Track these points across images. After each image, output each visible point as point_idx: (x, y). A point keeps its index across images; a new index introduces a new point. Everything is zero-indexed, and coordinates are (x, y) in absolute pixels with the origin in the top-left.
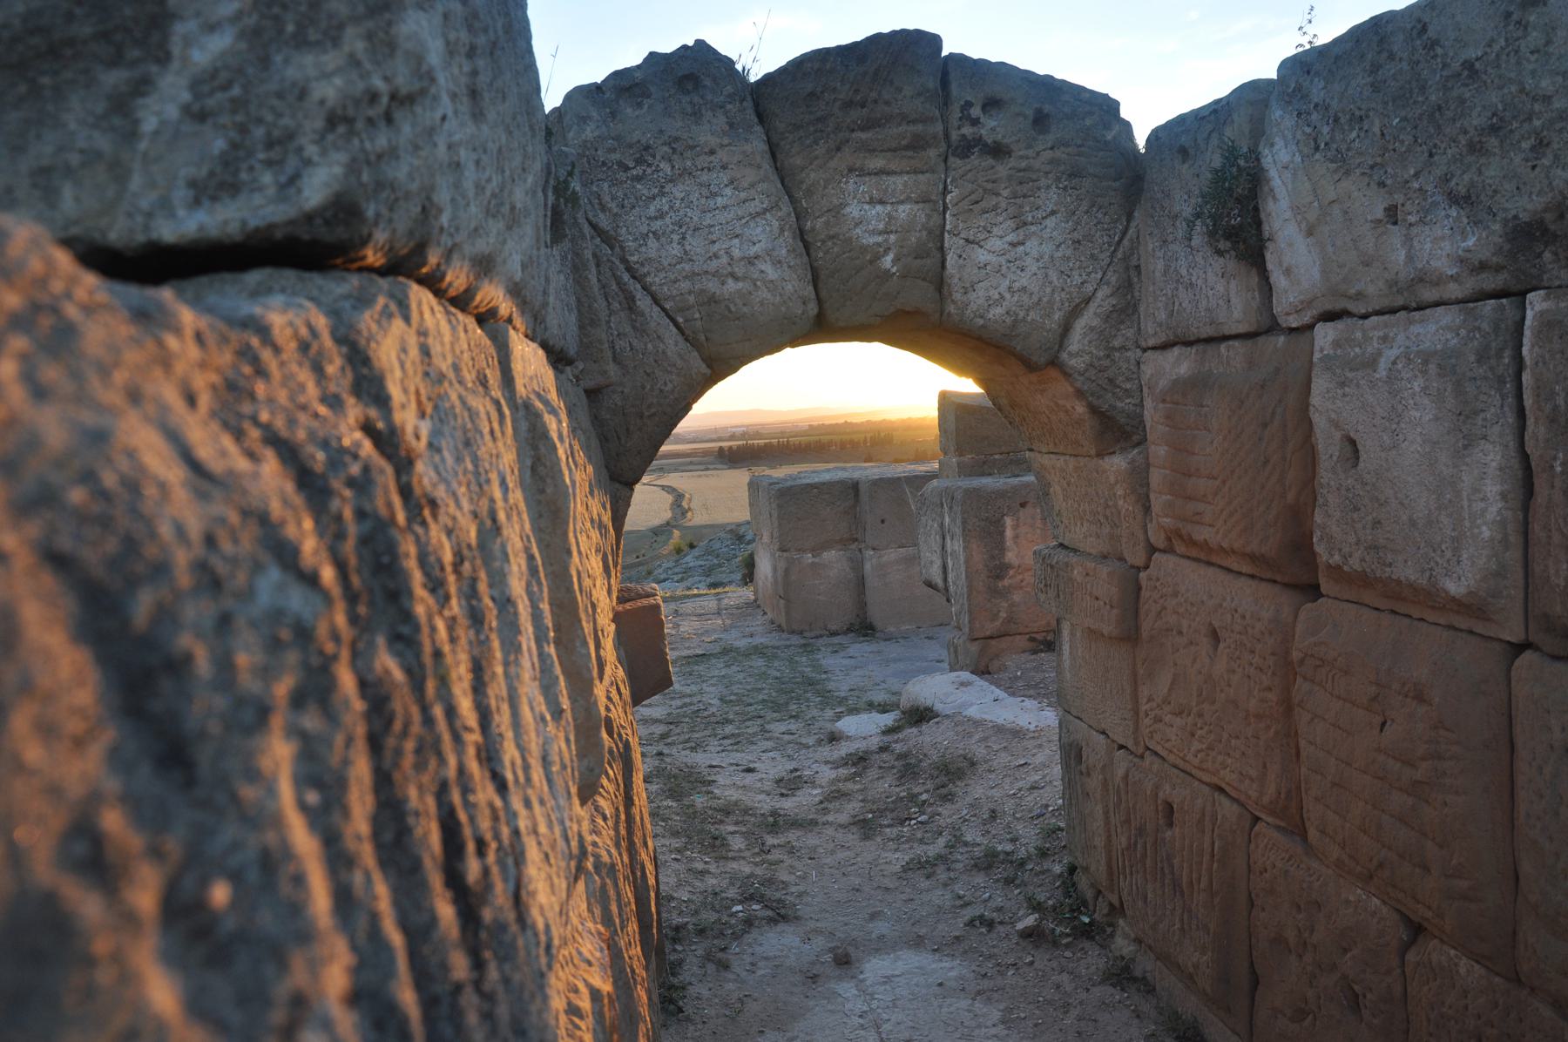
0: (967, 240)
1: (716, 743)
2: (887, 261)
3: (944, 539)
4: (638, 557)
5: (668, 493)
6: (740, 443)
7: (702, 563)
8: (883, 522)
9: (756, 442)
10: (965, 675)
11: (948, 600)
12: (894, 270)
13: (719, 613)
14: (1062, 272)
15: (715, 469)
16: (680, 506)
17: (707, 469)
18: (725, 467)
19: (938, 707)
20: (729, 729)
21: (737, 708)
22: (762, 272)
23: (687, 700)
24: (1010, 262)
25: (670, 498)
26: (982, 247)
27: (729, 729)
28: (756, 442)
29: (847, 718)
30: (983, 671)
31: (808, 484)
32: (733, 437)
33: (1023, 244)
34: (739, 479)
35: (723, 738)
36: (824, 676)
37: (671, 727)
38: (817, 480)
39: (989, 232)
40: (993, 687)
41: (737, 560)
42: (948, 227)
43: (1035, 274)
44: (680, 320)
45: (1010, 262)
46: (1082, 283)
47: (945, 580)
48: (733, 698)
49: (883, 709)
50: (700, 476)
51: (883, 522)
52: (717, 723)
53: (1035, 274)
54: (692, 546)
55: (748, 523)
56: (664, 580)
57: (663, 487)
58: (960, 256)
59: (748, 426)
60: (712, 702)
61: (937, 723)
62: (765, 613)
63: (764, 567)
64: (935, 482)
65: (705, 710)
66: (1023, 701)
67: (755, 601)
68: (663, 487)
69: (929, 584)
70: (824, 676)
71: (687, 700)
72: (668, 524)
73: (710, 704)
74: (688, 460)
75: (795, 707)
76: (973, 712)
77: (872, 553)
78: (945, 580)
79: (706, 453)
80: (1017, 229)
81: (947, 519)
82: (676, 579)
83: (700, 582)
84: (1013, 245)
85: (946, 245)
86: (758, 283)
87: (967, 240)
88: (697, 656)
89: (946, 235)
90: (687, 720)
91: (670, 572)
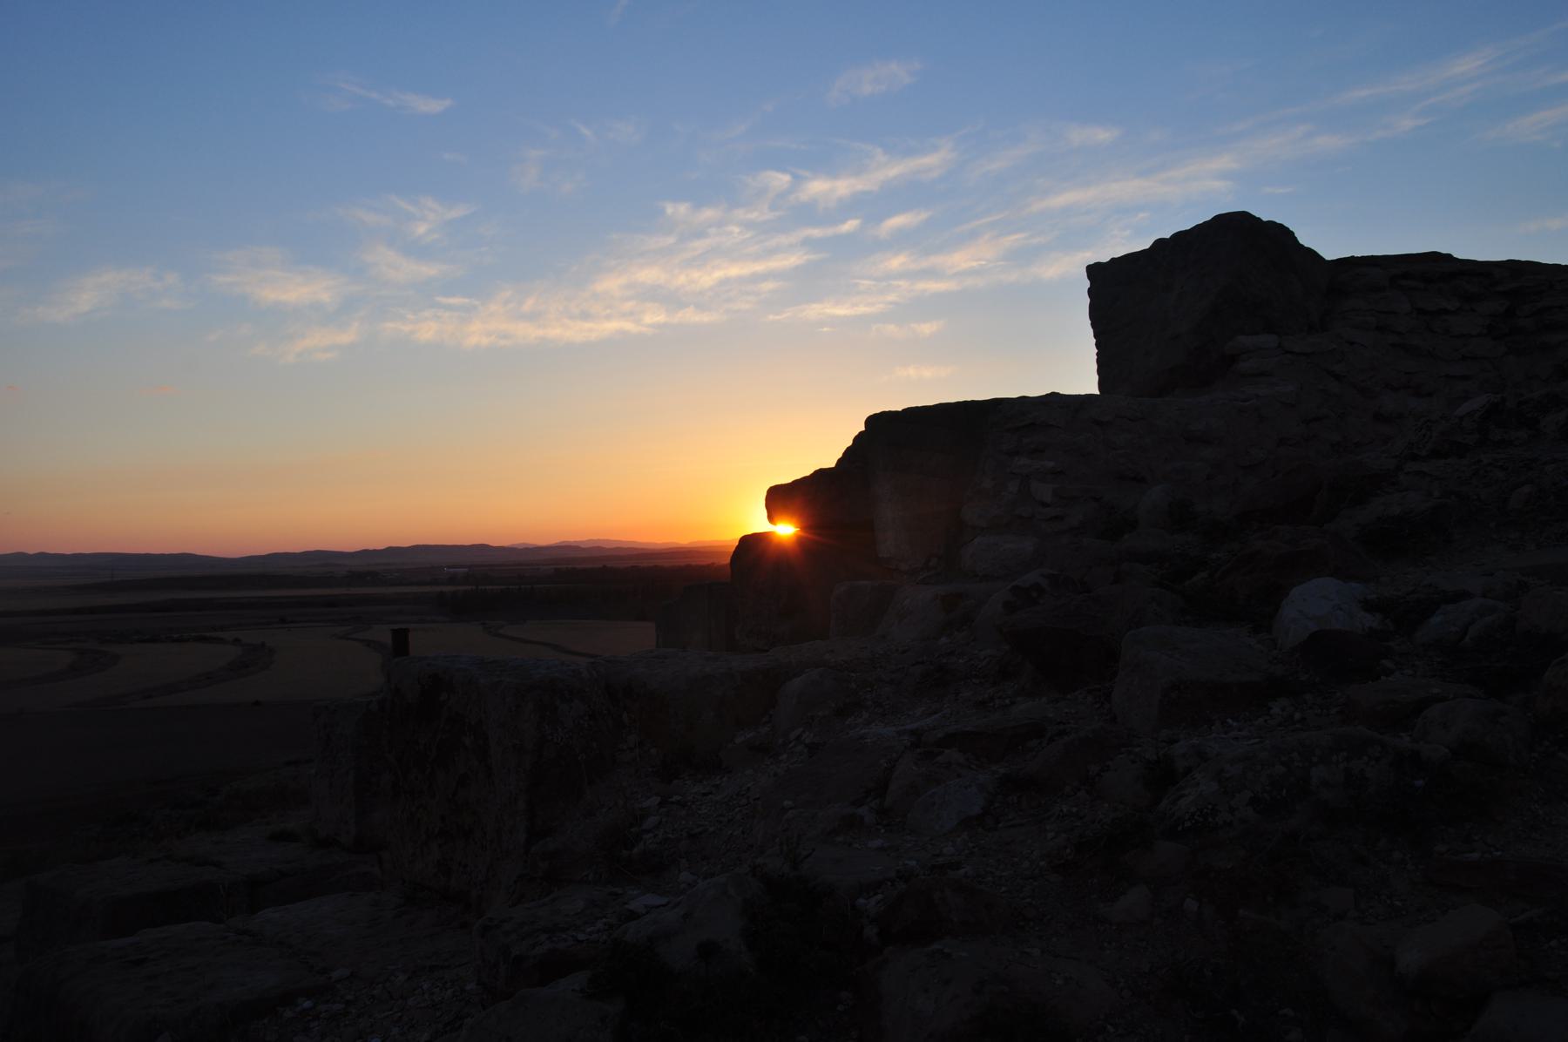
9: (487, 587)
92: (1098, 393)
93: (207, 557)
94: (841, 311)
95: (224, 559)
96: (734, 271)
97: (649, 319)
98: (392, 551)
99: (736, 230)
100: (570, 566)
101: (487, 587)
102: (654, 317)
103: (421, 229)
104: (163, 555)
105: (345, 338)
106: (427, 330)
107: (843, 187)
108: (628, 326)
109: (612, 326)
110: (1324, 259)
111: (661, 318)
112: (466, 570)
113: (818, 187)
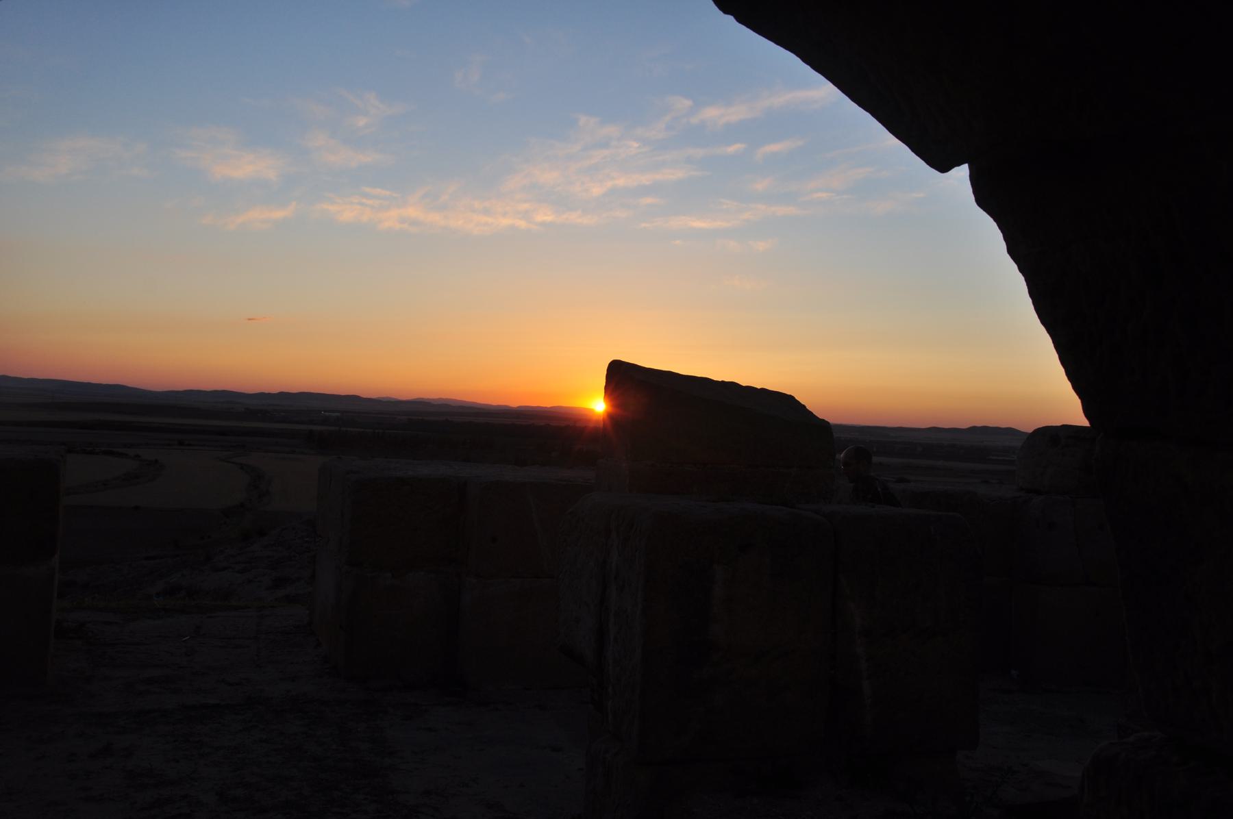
9: (349, 429)
92: (1084, 422)
93: (136, 389)
94: (698, 224)
95: (150, 392)
96: (621, 182)
97: (540, 218)
98: (284, 396)
99: (636, 145)
100: (420, 418)
101: (349, 429)
102: (545, 216)
103: (362, 122)
104: (89, 384)
105: (279, 214)
106: (347, 211)
107: (736, 113)
108: (522, 224)
109: (506, 222)
110: (756, 389)
111: (549, 218)
112: (338, 414)
113: (711, 113)
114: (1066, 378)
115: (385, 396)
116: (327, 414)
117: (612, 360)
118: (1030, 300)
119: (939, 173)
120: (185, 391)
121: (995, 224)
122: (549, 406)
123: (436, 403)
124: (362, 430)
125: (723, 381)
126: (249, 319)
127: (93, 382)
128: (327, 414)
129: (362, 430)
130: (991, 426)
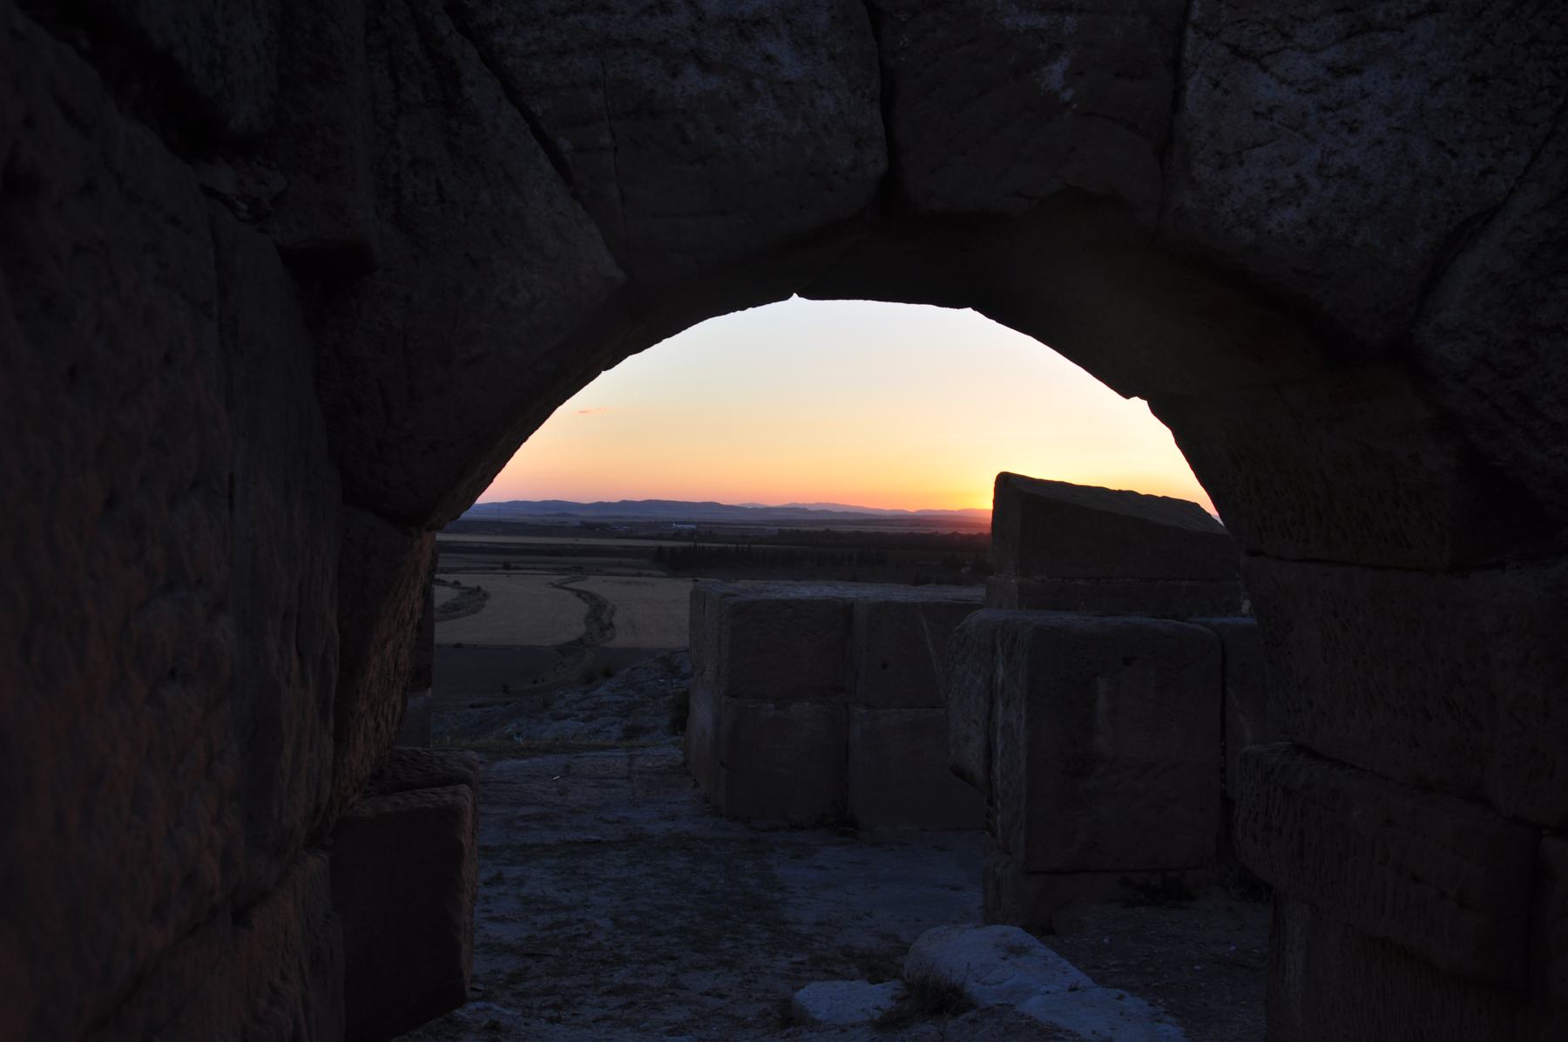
0: (1235, 50)
1: (596, 1000)
2: (1055, 73)
3: (992, 703)
4: (535, 682)
5: (585, 600)
6: (687, 544)
7: (618, 698)
8: (884, 666)
9: (706, 545)
10: (1015, 934)
11: (991, 802)
12: (1068, 95)
13: (628, 778)
14: (1441, 144)
15: (650, 575)
16: (598, 619)
17: (639, 575)
18: (664, 574)
19: (972, 987)
20: (620, 976)
21: (638, 938)
22: (769, 58)
23: (562, 916)
24: (1325, 109)
25: (584, 608)
26: (1265, 69)
27: (620, 976)
28: (706, 545)
29: (813, 985)
30: (1044, 930)
31: (778, 601)
32: (677, 536)
33: (1359, 72)
34: (678, 591)
35: (609, 993)
36: (778, 896)
37: (530, 962)
38: (792, 595)
39: (1285, 36)
40: (1065, 963)
41: (666, 699)
42: (1196, 15)
43: (1380, 142)
44: (565, 145)
45: (1325, 109)
46: (1483, 173)
47: (989, 768)
48: (633, 919)
49: (875, 970)
50: (629, 583)
51: (884, 666)
52: (604, 962)
53: (1380, 142)
54: (608, 674)
55: (687, 651)
56: (566, 717)
57: (579, 593)
58: (1217, 85)
59: (698, 524)
60: (599, 922)
61: (973, 1021)
62: (697, 785)
63: (702, 714)
64: (981, 614)
65: (588, 936)
66: (1121, 997)
67: (684, 764)
68: (579, 593)
69: (960, 773)
70: (778, 896)
71: (562, 916)
72: (581, 641)
73: (596, 926)
74: (616, 560)
75: (729, 944)
76: (1033, 1006)
77: (864, 711)
78: (989, 768)
79: (639, 553)
80: (1349, 36)
81: (1001, 673)
82: (582, 715)
83: (614, 724)
84: (1336, 71)
85: (1188, 54)
86: (757, 83)
87: (1235, 50)
88: (588, 842)
89: (1190, 34)
90: (557, 951)
91: (574, 707)
98: (625, 504)
100: (795, 528)
110: (1157, 497)
114: (993, 485)
115: (813, 501)
116: (680, 526)
117: (998, 473)
118: (531, 438)
119: (1124, 399)
120: (509, 503)
121: (560, 409)
122: (914, 511)
123: (750, 507)
124: (723, 545)
125: (1120, 491)
126: (581, 412)
127: (613, 501)
128: (680, 526)
129: (723, 545)
130: (639, 500)
